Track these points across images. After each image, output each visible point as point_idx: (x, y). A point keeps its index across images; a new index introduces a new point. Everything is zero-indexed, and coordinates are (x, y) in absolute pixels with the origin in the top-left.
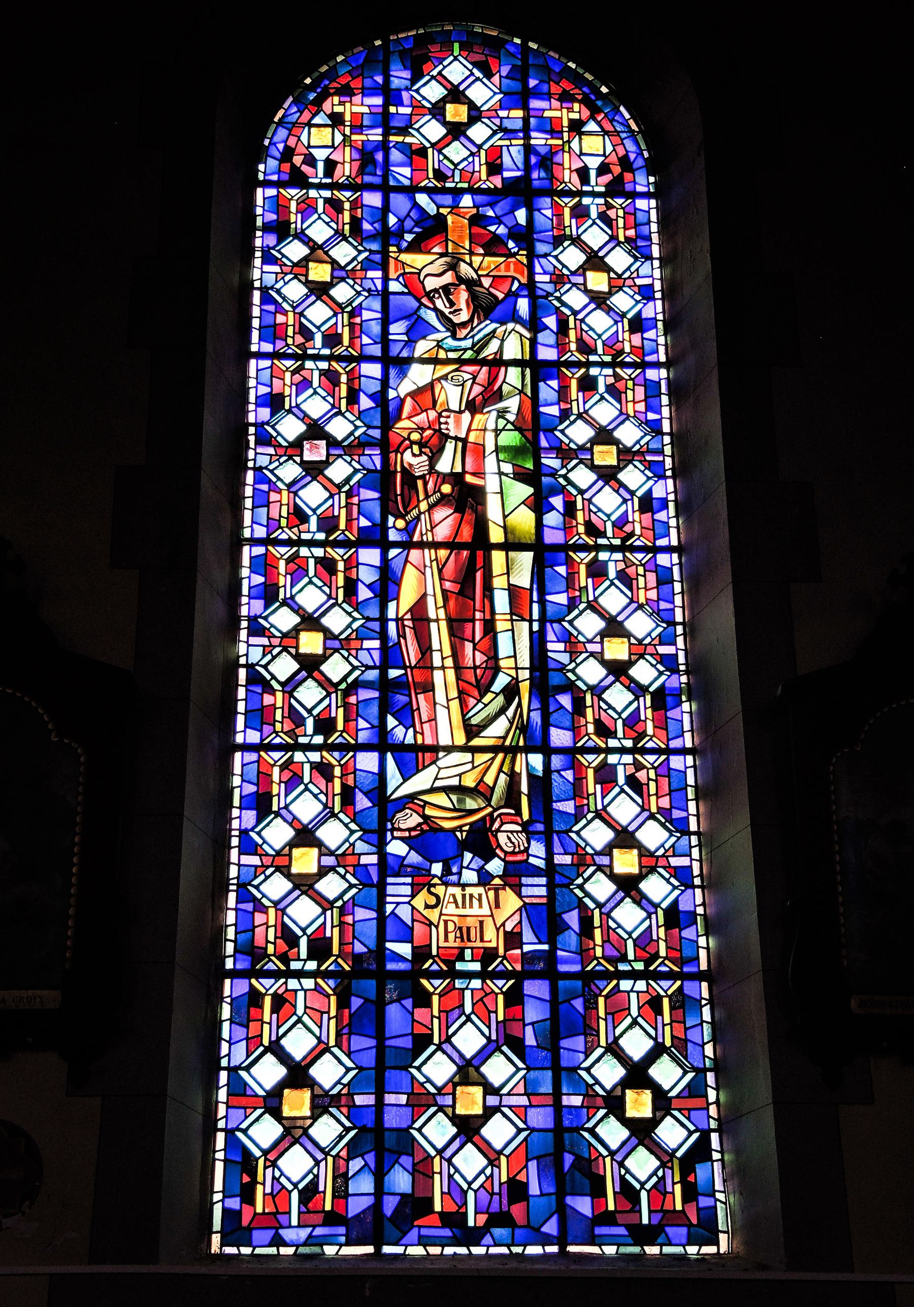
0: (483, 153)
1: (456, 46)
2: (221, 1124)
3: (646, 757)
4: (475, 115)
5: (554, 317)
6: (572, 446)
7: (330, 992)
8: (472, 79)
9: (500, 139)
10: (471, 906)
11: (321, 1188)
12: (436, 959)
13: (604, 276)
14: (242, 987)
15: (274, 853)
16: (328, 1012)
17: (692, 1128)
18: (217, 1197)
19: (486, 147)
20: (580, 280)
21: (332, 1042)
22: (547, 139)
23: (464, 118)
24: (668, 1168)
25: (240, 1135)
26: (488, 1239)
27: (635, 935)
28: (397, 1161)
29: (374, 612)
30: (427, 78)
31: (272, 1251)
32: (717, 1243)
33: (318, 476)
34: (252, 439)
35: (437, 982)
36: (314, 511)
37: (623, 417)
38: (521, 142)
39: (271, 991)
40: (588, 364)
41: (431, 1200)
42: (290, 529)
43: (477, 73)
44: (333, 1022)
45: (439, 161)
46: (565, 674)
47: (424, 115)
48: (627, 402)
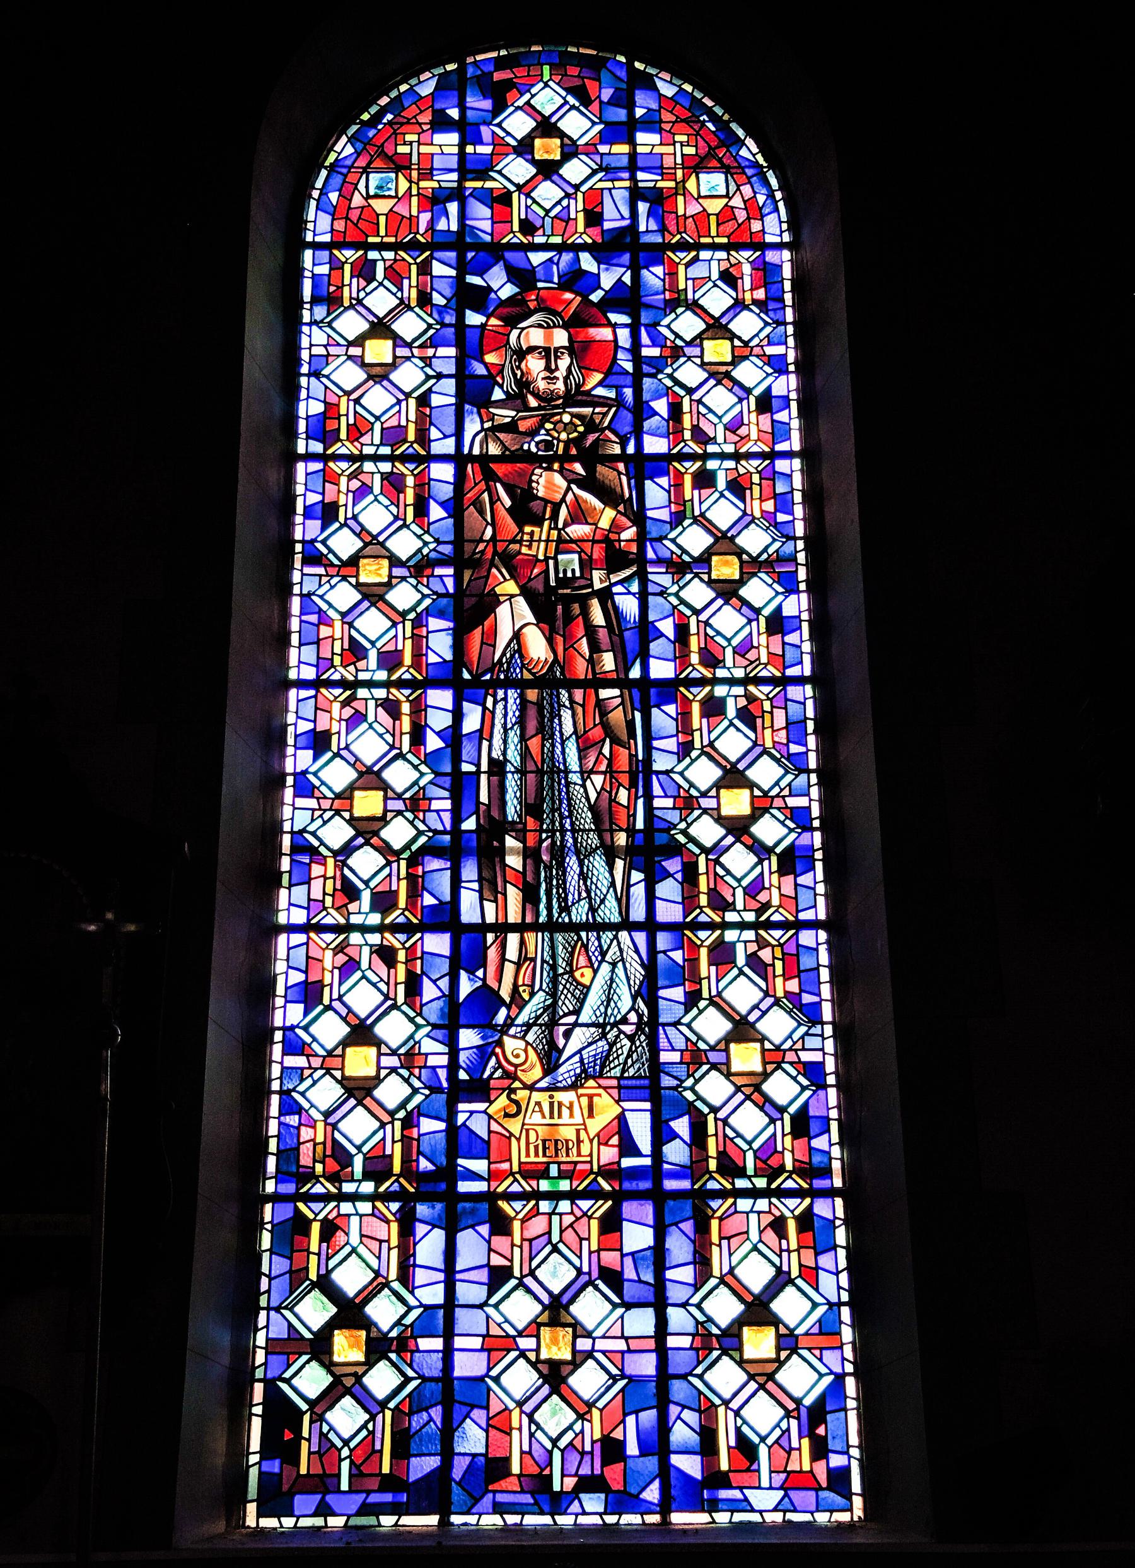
0: (580, 196)
1: (546, 69)
2: (259, 1374)
3: (771, 932)
4: (571, 150)
5: (686, 1119)
6: (686, 558)
7: (391, 1217)
8: (567, 107)
9: (600, 180)
10: (560, 1116)
11: (378, 1447)
12: (518, 1176)
13: (726, 344)
14: (286, 1211)
15: (325, 1054)
16: (388, 1241)
17: (824, 1370)
18: (254, 1459)
19: (584, 188)
20: (696, 351)
21: (393, 1275)
22: (656, 181)
23: (557, 156)
24: (794, 1417)
25: (284, 1386)
26: (575, 1507)
27: (756, 1145)
28: (468, 1416)
29: (450, 319)
30: (511, 109)
31: (319, 1521)
32: (851, 1510)
33: (364, 1098)
34: (298, 558)
35: (518, 1205)
36: (366, 883)
37: (746, 520)
38: (627, 184)
39: (320, 1217)
40: (725, 926)
41: (507, 1460)
42: (345, 667)
43: (571, 100)
44: (394, 1254)
45: (527, 207)
46: (680, 1093)
47: (507, 155)
48: (764, 729)
